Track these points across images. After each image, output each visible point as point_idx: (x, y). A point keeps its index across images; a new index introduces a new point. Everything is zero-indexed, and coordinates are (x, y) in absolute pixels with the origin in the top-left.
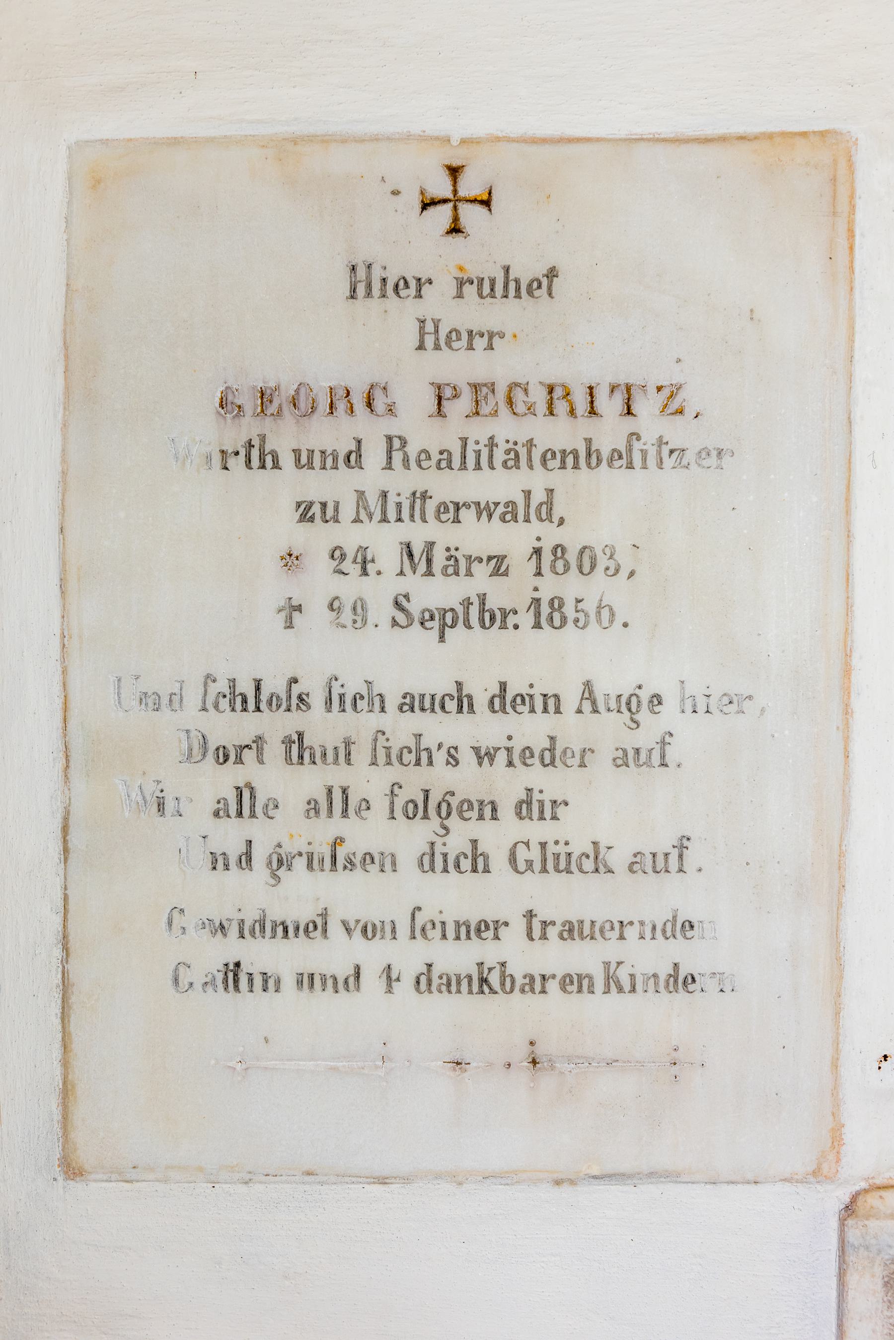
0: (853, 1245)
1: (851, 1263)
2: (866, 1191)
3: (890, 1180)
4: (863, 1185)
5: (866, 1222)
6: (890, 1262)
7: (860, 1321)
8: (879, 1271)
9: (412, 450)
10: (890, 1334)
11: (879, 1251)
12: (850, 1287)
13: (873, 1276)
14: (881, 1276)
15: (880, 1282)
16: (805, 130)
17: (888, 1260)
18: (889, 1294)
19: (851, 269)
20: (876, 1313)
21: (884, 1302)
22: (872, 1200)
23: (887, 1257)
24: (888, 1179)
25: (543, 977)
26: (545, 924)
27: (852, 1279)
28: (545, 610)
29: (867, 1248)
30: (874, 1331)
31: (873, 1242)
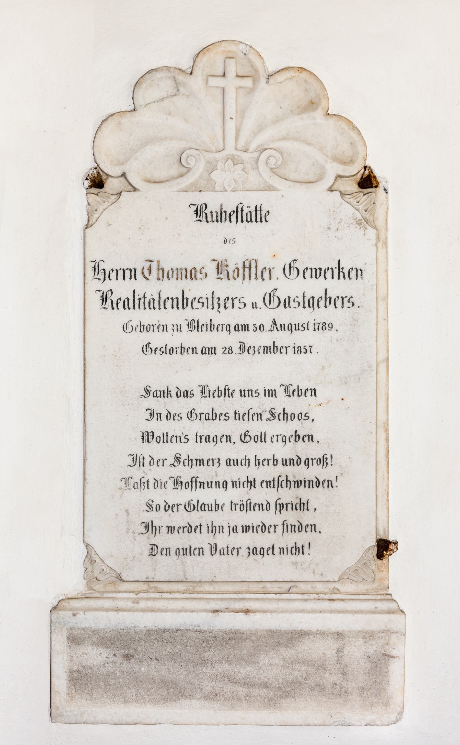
0: (53, 622)
1: (53, 630)
2: (63, 600)
3: (75, 596)
4: (63, 597)
5: (59, 612)
6: (69, 629)
7: (57, 654)
8: (65, 633)
9: (231, 269)
10: (70, 660)
11: (65, 624)
12: (53, 640)
13: (62, 635)
14: (66, 635)
15: (66, 638)
16: (86, 213)
17: (68, 628)
18: (70, 643)
19: (367, 221)
20: (64, 651)
21: (67, 646)
22: (64, 604)
23: (68, 627)
24: (74, 595)
25: (159, 527)
26: (235, 504)
27: (54, 637)
28: (296, 349)
29: (60, 623)
30: (63, 659)
31: (62, 620)
